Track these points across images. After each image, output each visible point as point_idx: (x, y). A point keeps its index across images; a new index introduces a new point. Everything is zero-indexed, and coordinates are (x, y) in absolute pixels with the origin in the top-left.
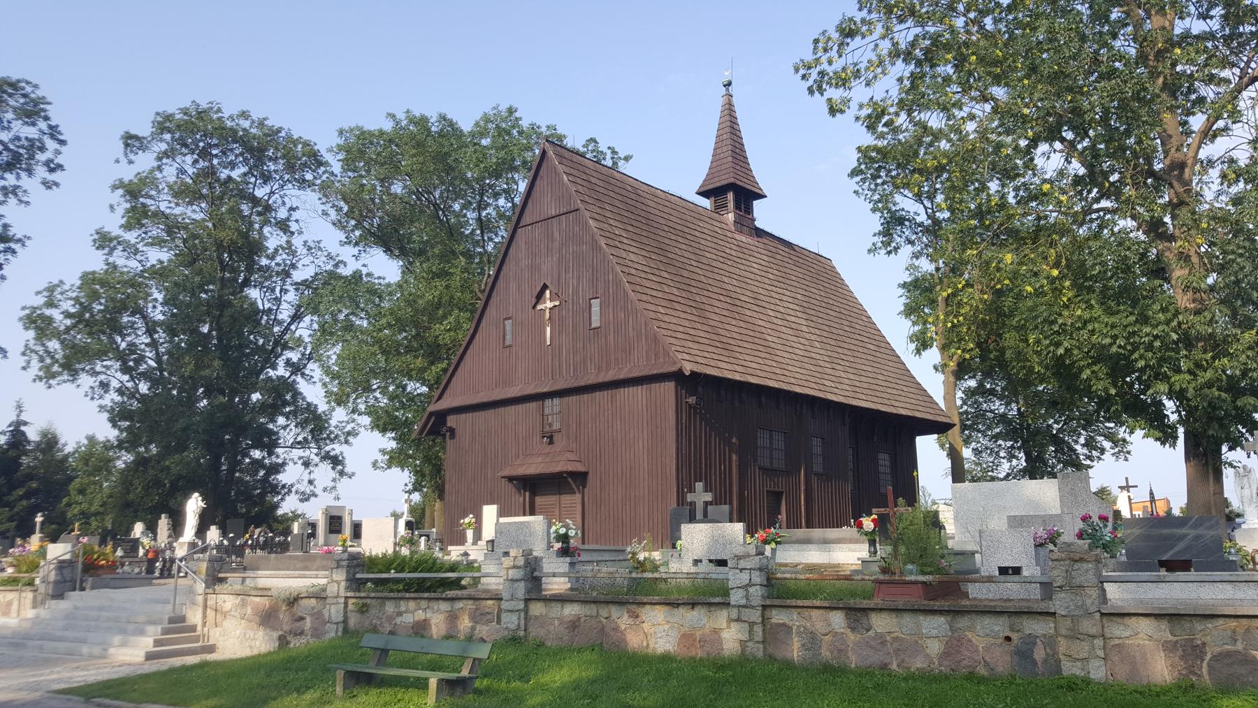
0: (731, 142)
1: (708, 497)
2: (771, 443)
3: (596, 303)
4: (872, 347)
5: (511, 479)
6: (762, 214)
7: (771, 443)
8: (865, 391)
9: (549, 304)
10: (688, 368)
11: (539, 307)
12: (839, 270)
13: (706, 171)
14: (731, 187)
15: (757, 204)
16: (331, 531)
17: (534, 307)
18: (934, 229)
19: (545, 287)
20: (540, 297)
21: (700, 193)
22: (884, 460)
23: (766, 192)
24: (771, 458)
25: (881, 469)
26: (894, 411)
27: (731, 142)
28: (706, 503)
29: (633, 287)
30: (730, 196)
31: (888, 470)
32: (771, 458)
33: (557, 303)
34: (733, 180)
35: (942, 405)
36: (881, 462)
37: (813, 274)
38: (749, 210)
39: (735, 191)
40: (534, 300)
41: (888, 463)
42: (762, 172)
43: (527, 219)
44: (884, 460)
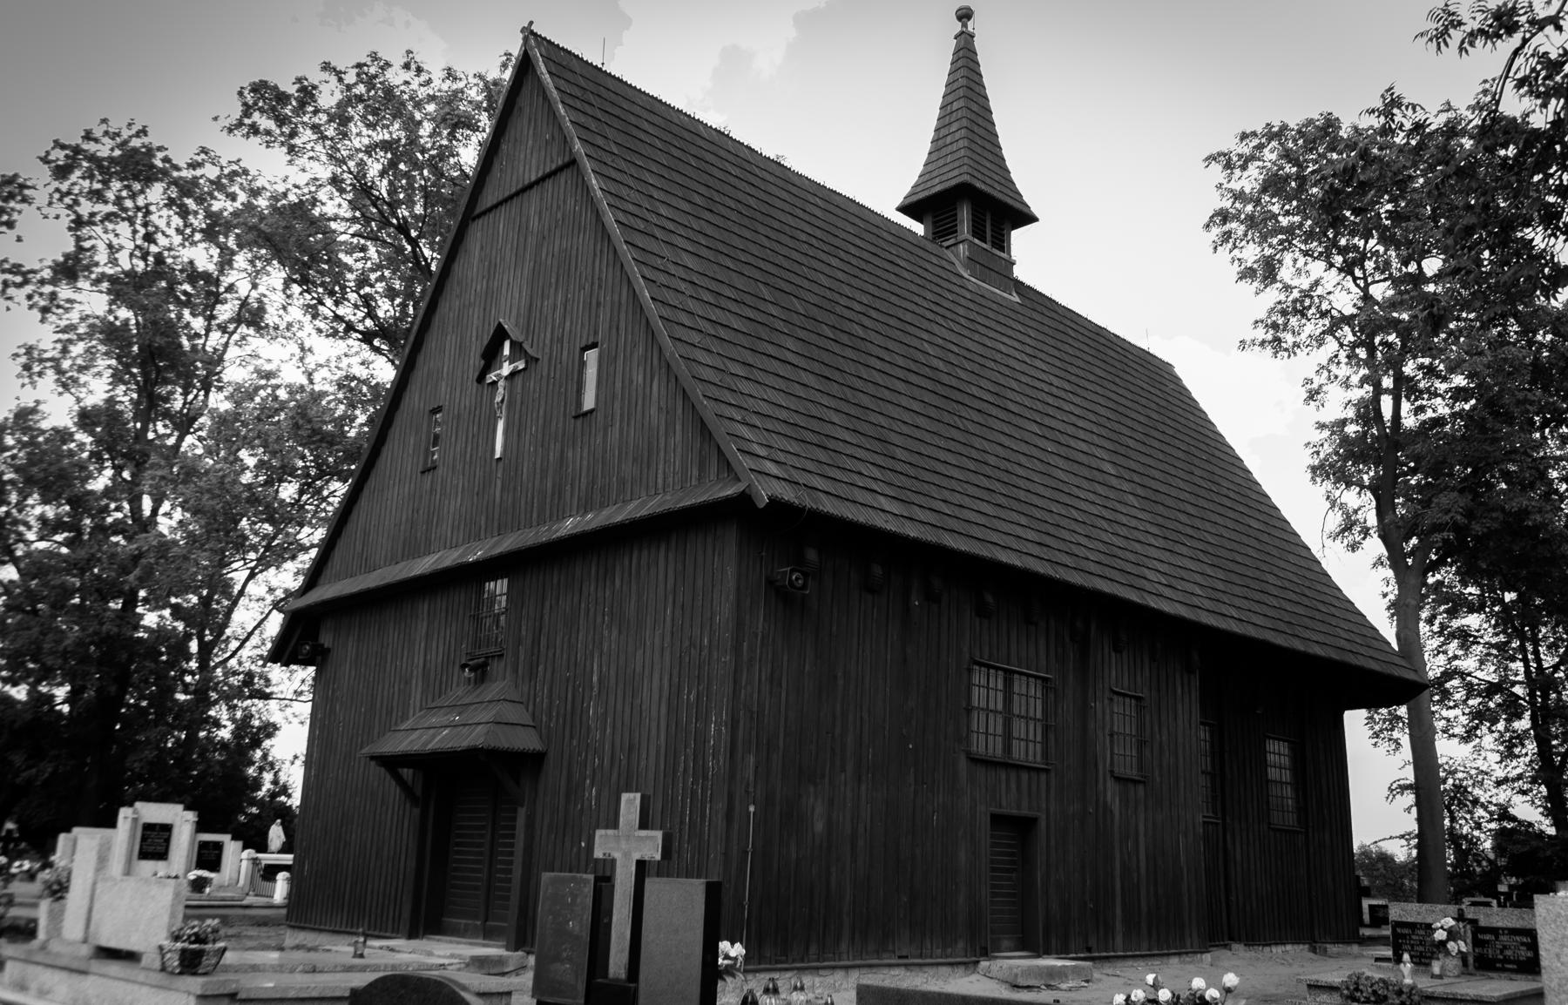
0: (967, 109)
1: (650, 846)
2: (1008, 700)
3: (592, 356)
4: (1256, 525)
5: (372, 758)
6: (1033, 258)
7: (1008, 700)
8: (1237, 602)
9: (506, 369)
10: (764, 492)
11: (492, 377)
12: (1187, 383)
13: (920, 168)
14: (963, 192)
15: (1019, 238)
16: (144, 855)
17: (481, 378)
18: (1368, 323)
19: (500, 335)
20: (491, 356)
21: (903, 209)
22: (1278, 754)
23: (1035, 210)
24: (1008, 737)
25: (1273, 773)
26: (1298, 645)
27: (967, 109)
28: (641, 865)
29: (666, 312)
30: (965, 215)
31: (1287, 776)
32: (1008, 737)
33: (521, 365)
34: (966, 178)
35: (1395, 646)
36: (1271, 758)
37: (1138, 395)
38: (1002, 243)
39: (973, 202)
40: (476, 362)
41: (1285, 761)
42: (1027, 173)
43: (489, 198)
44: (1278, 754)
